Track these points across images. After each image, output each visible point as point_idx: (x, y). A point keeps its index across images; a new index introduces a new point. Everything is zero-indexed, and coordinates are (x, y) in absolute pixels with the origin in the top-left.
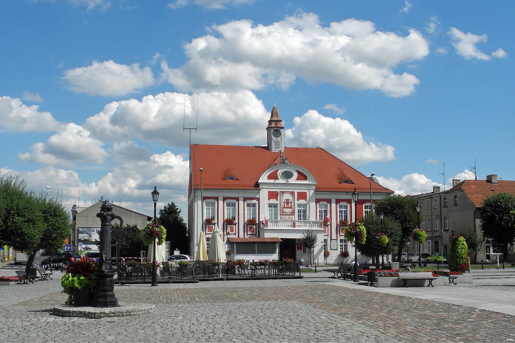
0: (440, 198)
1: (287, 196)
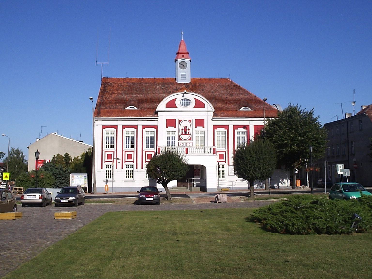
0: (347, 123)
1: (185, 124)
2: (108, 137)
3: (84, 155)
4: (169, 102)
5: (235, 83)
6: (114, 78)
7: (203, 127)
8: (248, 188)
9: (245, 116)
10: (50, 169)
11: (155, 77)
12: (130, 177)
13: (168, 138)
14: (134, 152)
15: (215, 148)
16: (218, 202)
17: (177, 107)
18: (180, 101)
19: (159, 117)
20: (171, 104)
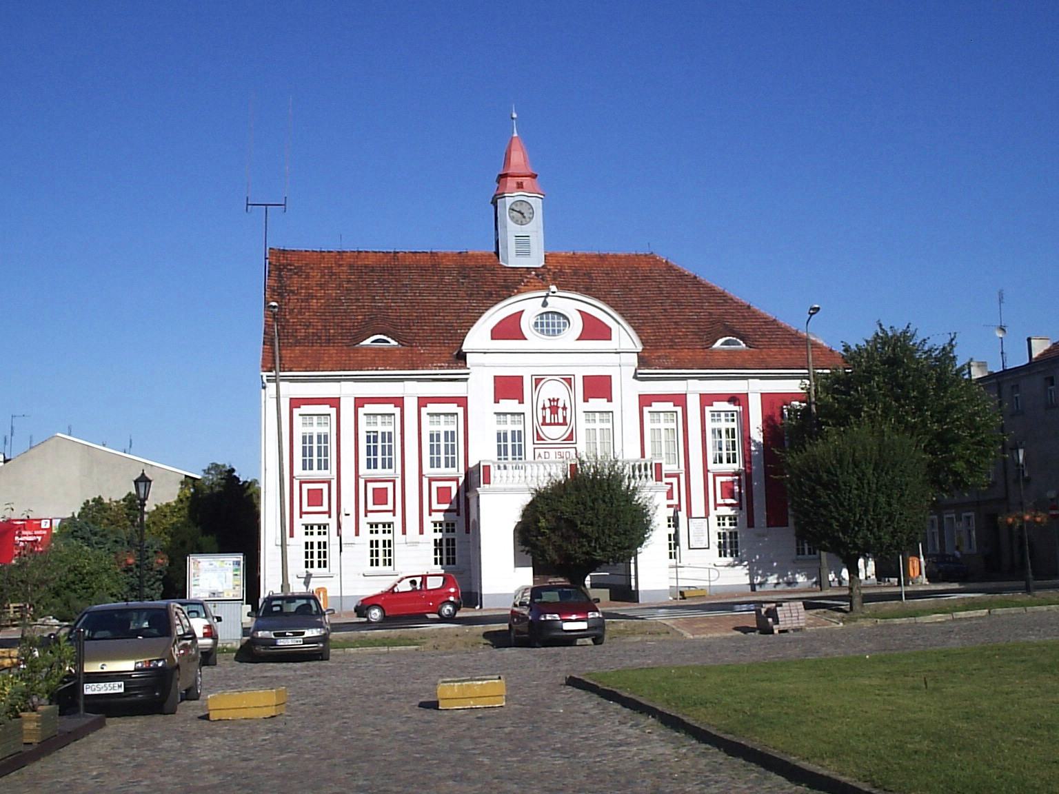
1: (554, 390)
2: (435, 433)
3: (187, 498)
4: (500, 322)
5: (680, 266)
6: (306, 251)
7: (608, 401)
8: (749, 587)
9: (731, 364)
10: (96, 543)
11: (434, 251)
12: (381, 562)
13: (499, 434)
14: (394, 481)
15: (661, 464)
16: (776, 632)
17: (526, 339)
18: (535, 320)
19: (472, 368)
20: (509, 329)
